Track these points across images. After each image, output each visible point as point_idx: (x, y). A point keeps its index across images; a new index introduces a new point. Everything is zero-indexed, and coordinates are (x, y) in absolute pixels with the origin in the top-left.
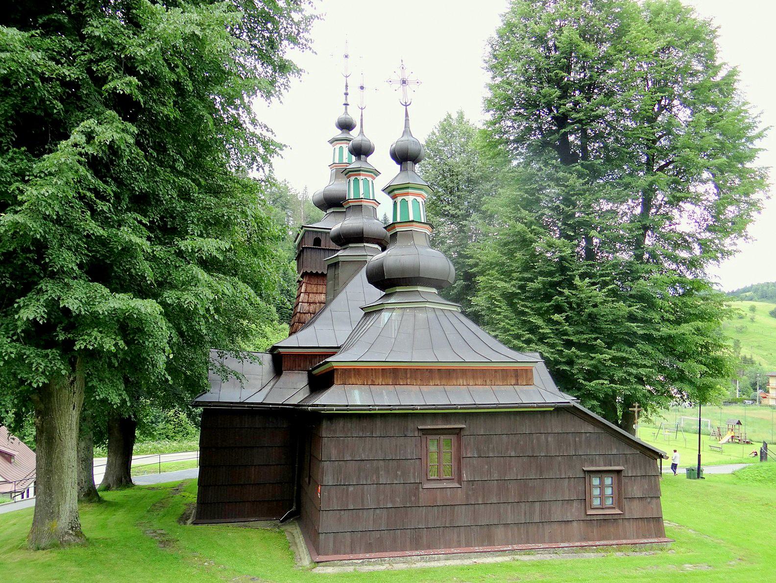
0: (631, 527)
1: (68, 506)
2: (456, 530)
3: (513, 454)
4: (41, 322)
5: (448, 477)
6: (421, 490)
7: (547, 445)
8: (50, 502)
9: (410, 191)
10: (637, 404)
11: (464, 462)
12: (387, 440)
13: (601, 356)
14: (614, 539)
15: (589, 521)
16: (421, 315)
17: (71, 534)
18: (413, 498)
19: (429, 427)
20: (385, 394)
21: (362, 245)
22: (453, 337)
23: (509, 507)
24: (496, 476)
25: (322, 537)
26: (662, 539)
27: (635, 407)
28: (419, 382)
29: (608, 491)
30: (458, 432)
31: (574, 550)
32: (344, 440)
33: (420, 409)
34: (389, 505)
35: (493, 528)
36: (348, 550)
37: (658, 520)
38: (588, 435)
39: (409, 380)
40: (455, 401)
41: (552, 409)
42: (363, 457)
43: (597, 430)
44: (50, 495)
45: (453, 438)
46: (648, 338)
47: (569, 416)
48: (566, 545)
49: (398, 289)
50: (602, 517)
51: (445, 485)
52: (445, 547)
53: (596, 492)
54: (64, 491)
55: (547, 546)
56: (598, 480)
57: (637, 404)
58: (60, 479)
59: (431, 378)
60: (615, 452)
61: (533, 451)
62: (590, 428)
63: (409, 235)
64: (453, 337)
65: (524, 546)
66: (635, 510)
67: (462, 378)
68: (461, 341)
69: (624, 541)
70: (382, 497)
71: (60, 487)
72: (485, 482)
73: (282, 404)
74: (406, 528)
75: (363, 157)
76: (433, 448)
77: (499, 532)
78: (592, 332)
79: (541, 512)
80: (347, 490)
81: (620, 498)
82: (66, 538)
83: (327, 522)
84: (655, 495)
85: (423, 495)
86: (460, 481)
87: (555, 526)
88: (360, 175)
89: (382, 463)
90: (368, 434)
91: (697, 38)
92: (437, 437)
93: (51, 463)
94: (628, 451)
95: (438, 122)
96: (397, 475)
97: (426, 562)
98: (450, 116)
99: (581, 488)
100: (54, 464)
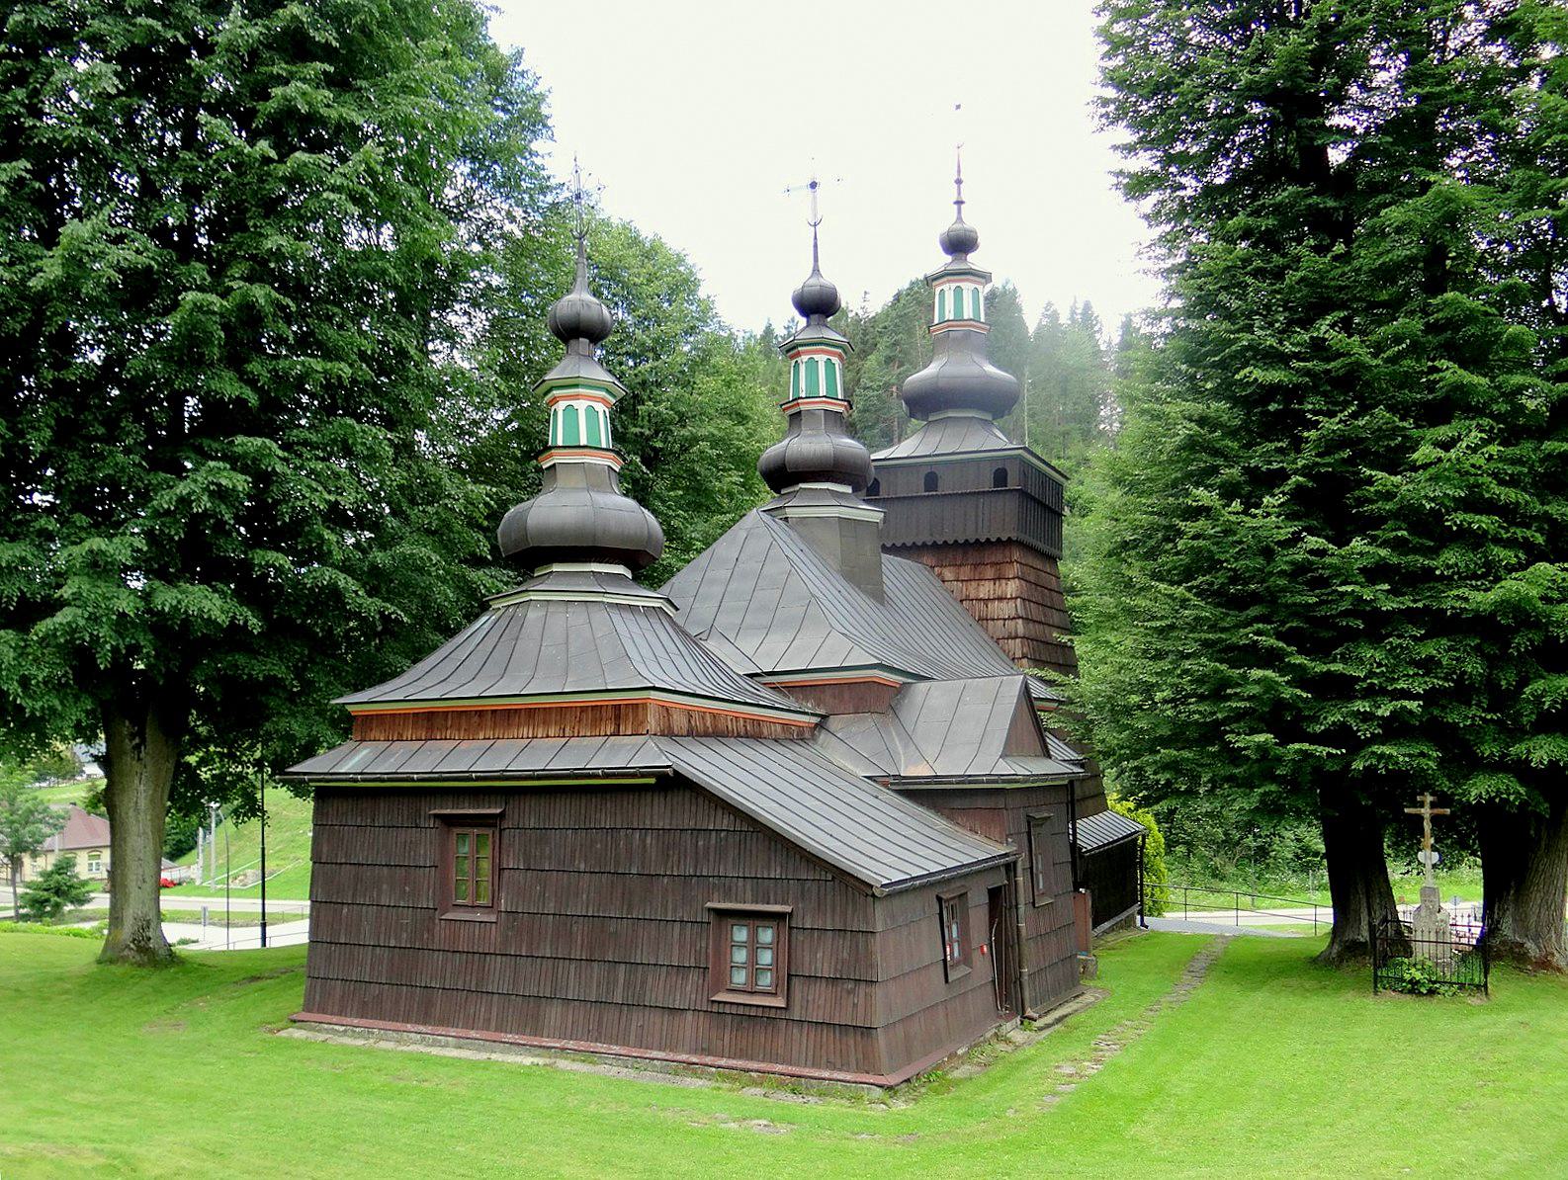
0: (801, 1039)
3: (582, 867)
4: (102, 667)
6: (437, 921)
9: (581, 390)
10: (1429, 798)
12: (393, 832)
15: (718, 1013)
24: (551, 908)
27: (1422, 805)
33: (419, 780)
38: (723, 834)
40: (557, 765)
46: (1439, 624)
48: (661, 1055)
50: (741, 1011)
53: (740, 956)
57: (1429, 798)
60: (776, 873)
61: (617, 863)
62: (725, 822)
65: (583, 1045)
66: (815, 1003)
79: (627, 985)
81: (789, 978)
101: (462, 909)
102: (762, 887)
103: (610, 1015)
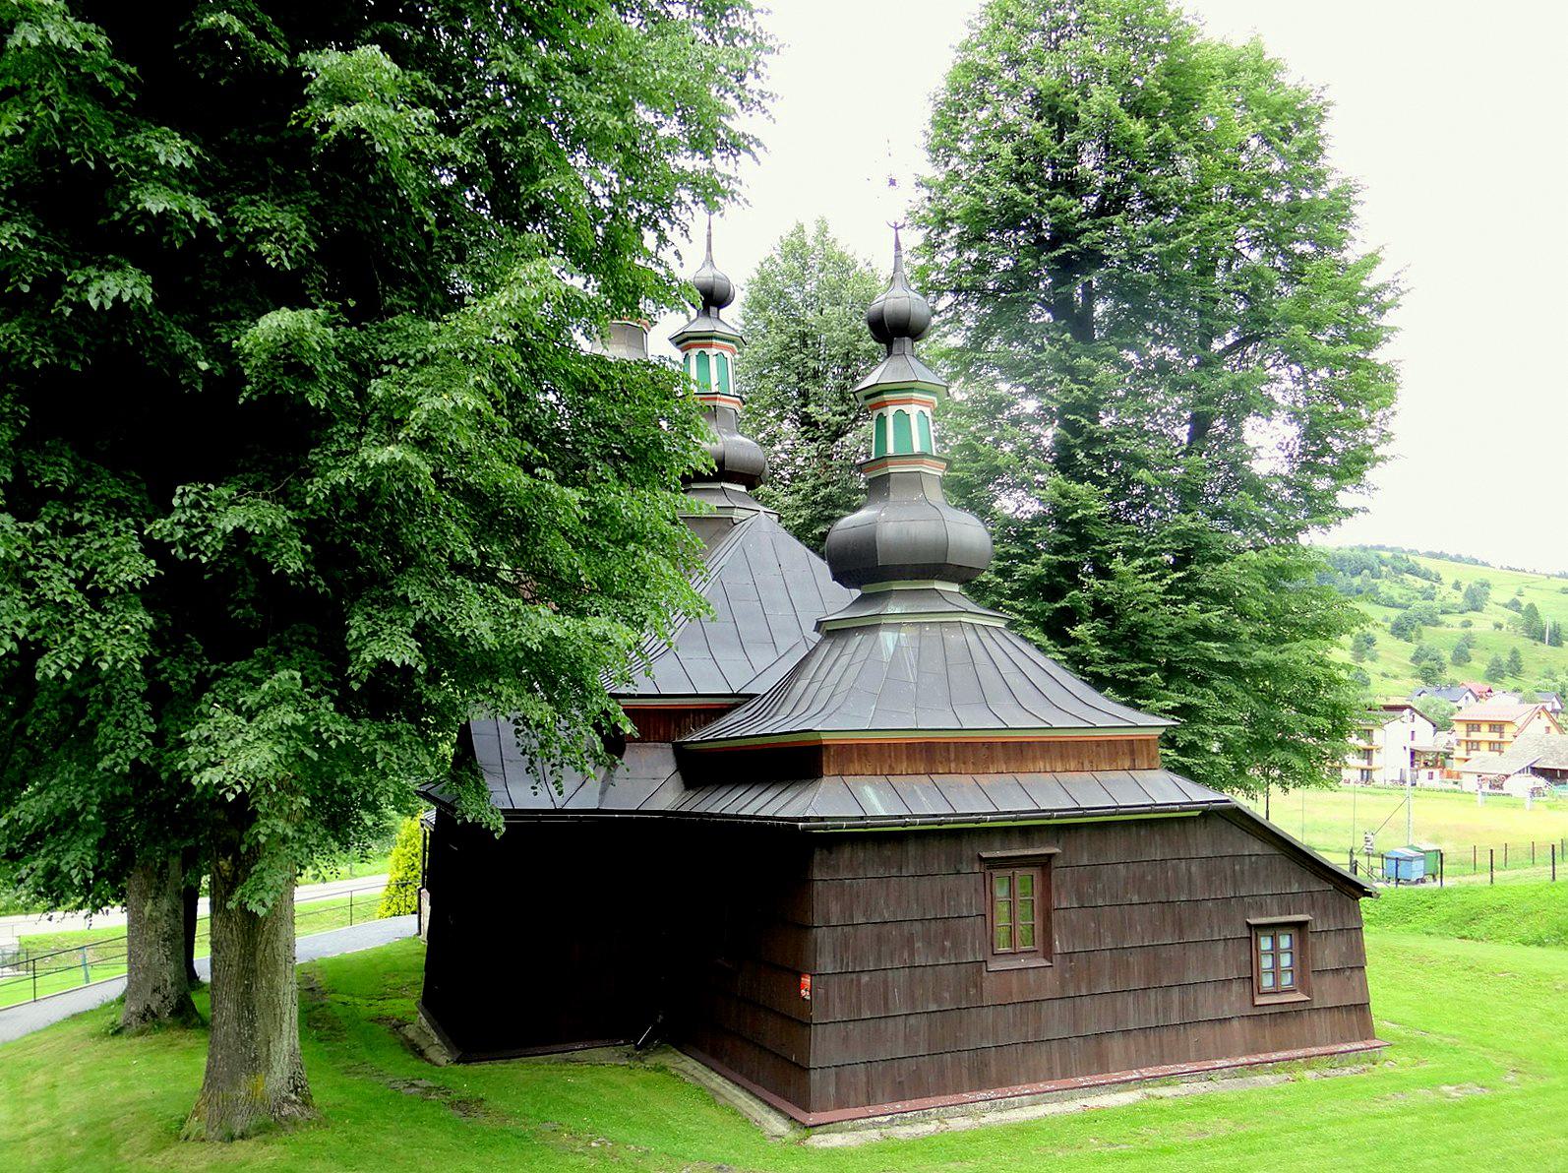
0: (1322, 1023)
1: (285, 1043)
2: (1044, 1047)
3: (1135, 899)
5: (1028, 948)
6: (985, 974)
7: (1190, 879)
8: (251, 1037)
9: (915, 395)
11: (1054, 916)
12: (926, 882)
13: (1159, 704)
14: (1297, 1048)
15: (1260, 1017)
16: (953, 638)
17: (295, 1102)
18: (972, 991)
19: (999, 854)
20: (919, 792)
21: (717, 486)
22: (1016, 681)
23: (1131, 998)
24: (1108, 942)
25: (815, 1076)
26: (1373, 1043)
28: (971, 768)
29: (1285, 961)
30: (1044, 863)
31: (1237, 1072)
32: (851, 886)
34: (933, 1007)
35: (1105, 1039)
36: (863, 1099)
37: (1362, 1008)
39: (953, 765)
41: (1197, 813)
42: (887, 916)
43: (1269, 850)
44: (251, 1023)
45: (1035, 872)
47: (1222, 825)
49: (897, 586)
50: (1277, 1009)
51: (1022, 963)
52: (1029, 1082)
54: (278, 1011)
55: (1196, 1068)
56: (1269, 940)
58: (271, 987)
59: (991, 759)
60: (1295, 888)
62: (1256, 847)
63: (915, 481)
64: (1016, 681)
66: (1328, 992)
67: (1043, 758)
68: (1029, 687)
69: (1315, 1050)
70: (919, 992)
71: (272, 1004)
72: (1091, 955)
73: (637, 812)
74: (960, 1054)
75: (713, 309)
76: (1001, 892)
77: (1116, 1046)
78: (1132, 658)
79: (1183, 1004)
80: (859, 981)
81: (1304, 971)
82: (287, 1110)
83: (825, 1048)
84: (1354, 964)
85: (989, 984)
86: (1048, 954)
87: (1204, 1030)
88: (710, 346)
89: (918, 926)
90: (894, 872)
91: (1293, 123)
92: (1010, 872)
93: (253, 955)
94: (1316, 886)
95: (777, 242)
96: (943, 949)
97: (1001, 1111)
98: (801, 228)
99: (1244, 957)
100: (259, 956)
101: (1003, 958)
102: (1286, 903)
103: (1168, 1036)
